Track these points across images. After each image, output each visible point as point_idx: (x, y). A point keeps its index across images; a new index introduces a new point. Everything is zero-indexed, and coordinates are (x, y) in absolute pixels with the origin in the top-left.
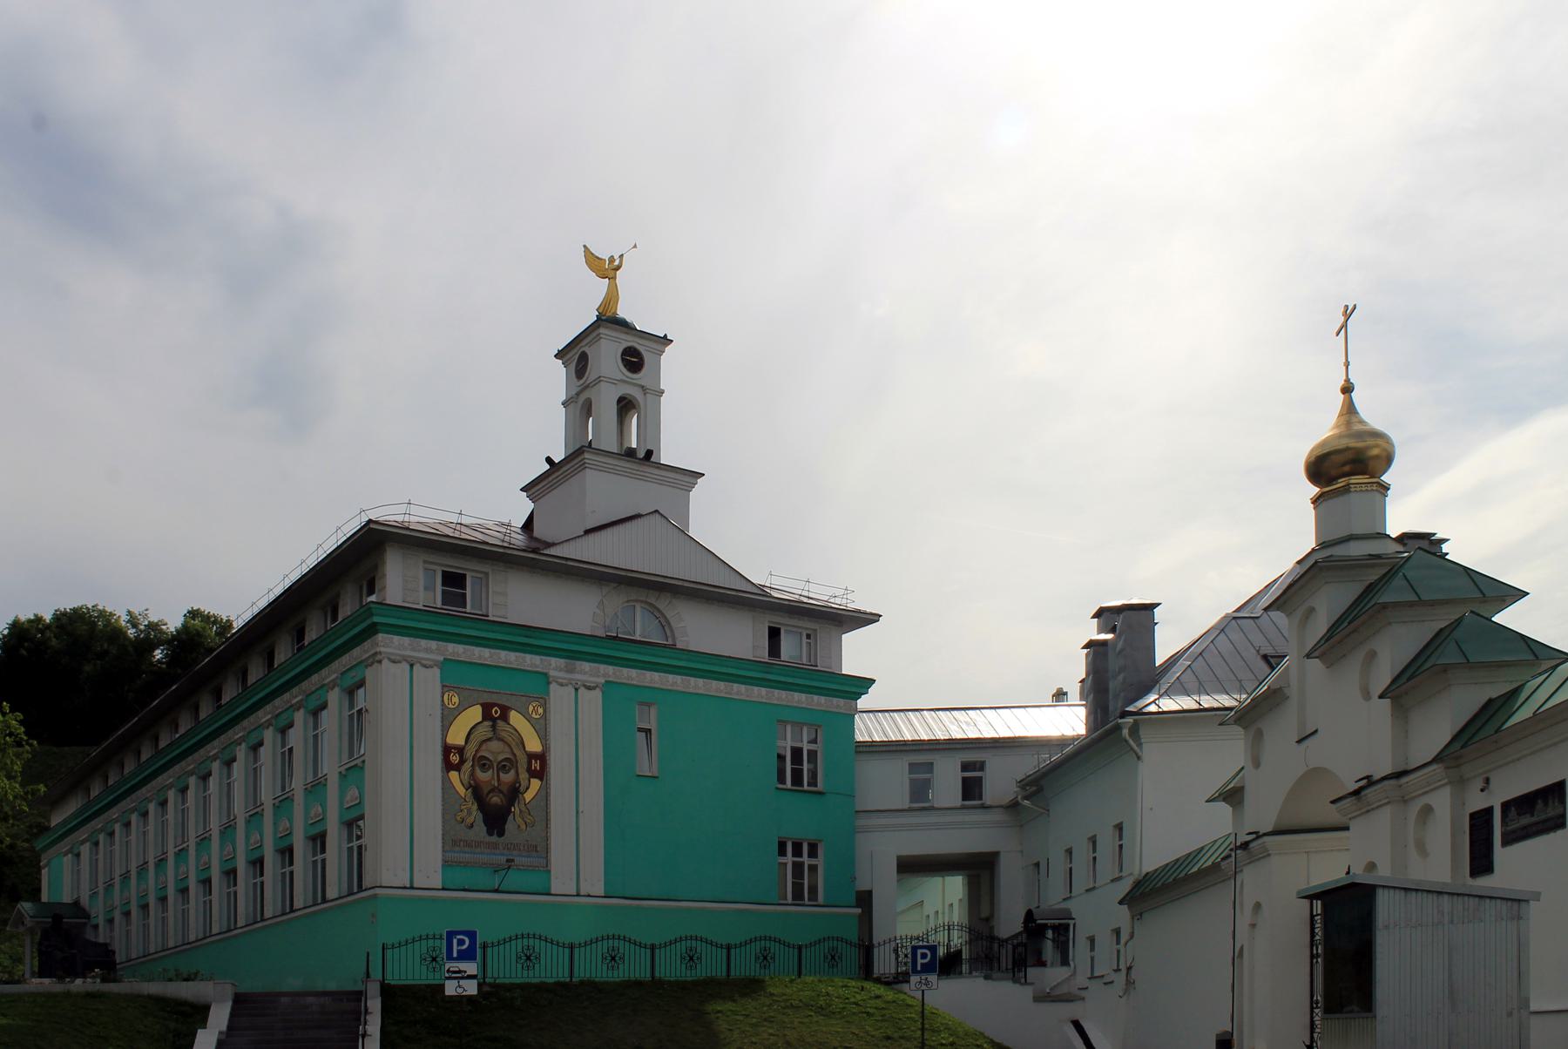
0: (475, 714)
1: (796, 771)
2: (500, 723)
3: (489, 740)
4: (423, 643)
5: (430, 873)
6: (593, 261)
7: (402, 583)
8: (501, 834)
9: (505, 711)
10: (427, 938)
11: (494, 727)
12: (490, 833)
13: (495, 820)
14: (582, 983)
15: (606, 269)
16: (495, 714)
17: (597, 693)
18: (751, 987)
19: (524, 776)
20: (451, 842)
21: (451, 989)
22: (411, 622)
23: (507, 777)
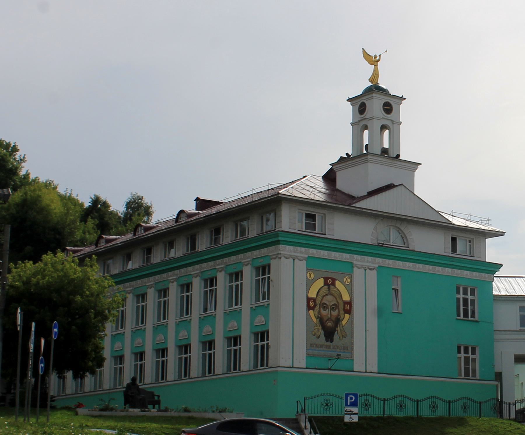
0: (321, 282)
1: (466, 310)
2: (332, 287)
3: (327, 295)
4: (299, 248)
5: (301, 361)
6: (366, 56)
7: (289, 221)
8: (332, 341)
9: (334, 280)
10: (318, 396)
11: (329, 288)
12: (327, 341)
13: (329, 335)
14: (389, 417)
15: (373, 61)
16: (329, 282)
17: (375, 272)
18: (460, 422)
19: (342, 312)
20: (310, 345)
21: (347, 419)
22: (294, 239)
23: (335, 313)
